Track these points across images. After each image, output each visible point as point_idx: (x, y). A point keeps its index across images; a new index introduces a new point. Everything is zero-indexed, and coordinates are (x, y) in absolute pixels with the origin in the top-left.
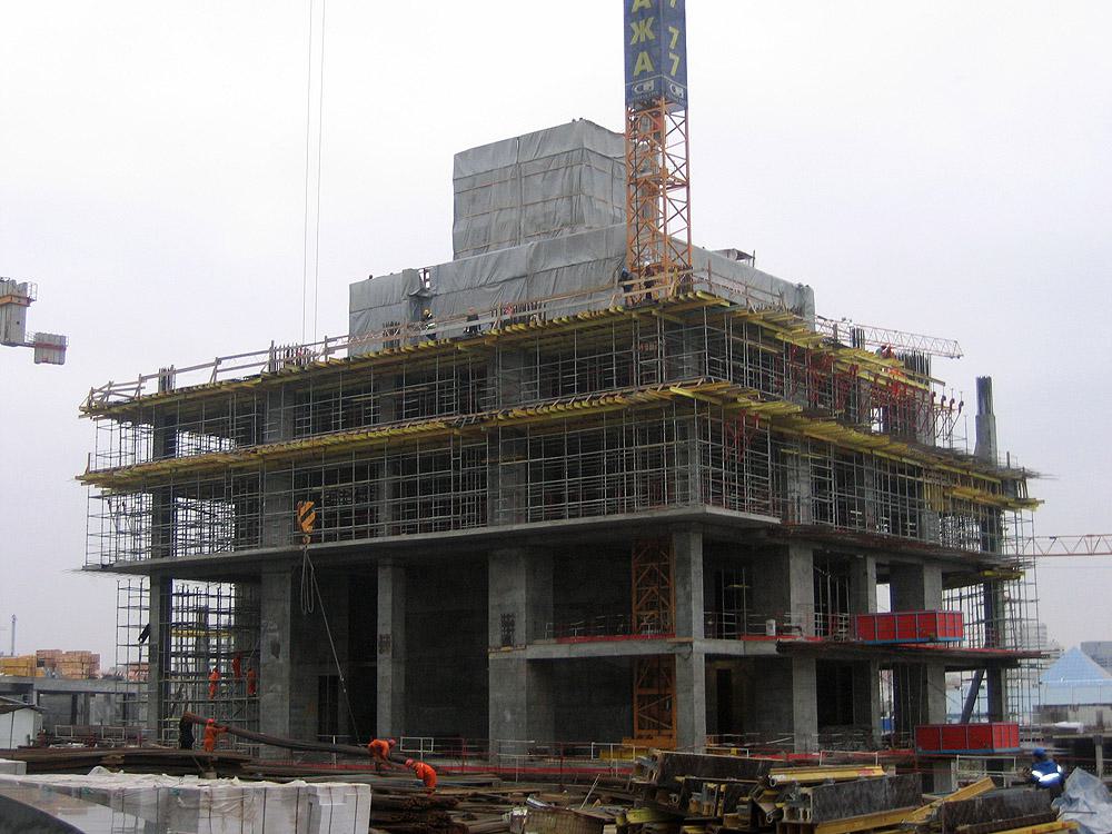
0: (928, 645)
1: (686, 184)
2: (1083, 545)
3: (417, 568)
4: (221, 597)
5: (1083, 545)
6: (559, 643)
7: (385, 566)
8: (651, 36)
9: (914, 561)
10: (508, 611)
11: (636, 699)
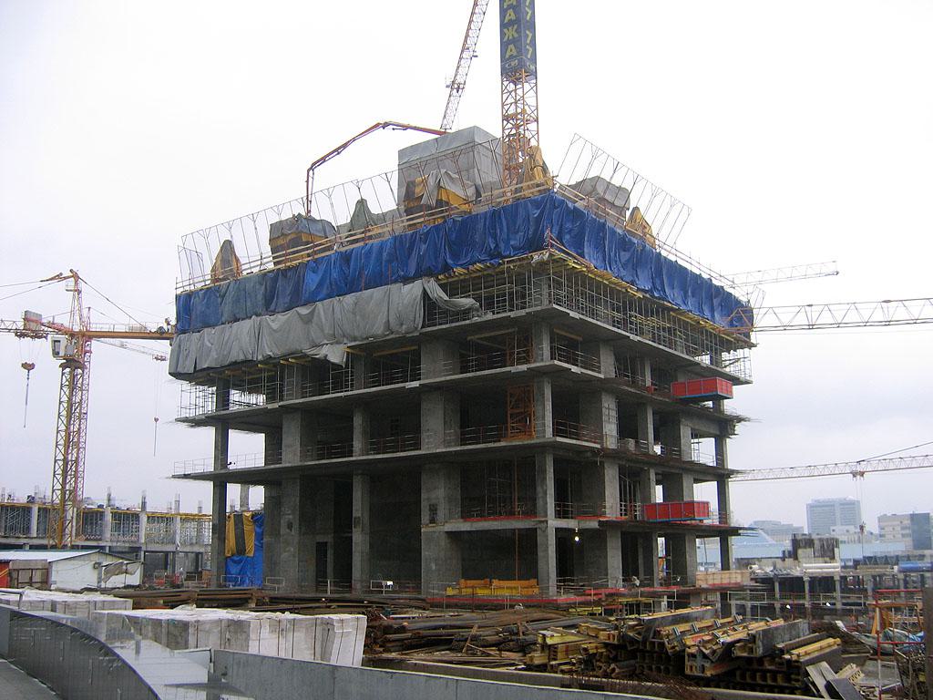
0: (689, 522)
1: (537, 120)
2: (802, 315)
3: (376, 476)
4: (257, 496)
5: (802, 315)
6: (465, 521)
7: (357, 475)
8: (516, 35)
9: (677, 471)
10: (433, 502)
11: (509, 415)
